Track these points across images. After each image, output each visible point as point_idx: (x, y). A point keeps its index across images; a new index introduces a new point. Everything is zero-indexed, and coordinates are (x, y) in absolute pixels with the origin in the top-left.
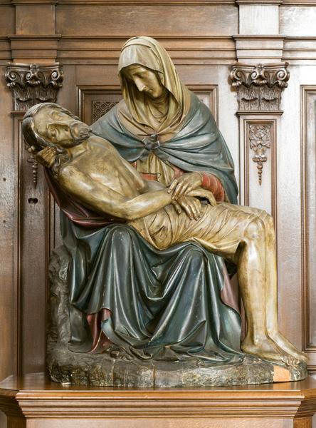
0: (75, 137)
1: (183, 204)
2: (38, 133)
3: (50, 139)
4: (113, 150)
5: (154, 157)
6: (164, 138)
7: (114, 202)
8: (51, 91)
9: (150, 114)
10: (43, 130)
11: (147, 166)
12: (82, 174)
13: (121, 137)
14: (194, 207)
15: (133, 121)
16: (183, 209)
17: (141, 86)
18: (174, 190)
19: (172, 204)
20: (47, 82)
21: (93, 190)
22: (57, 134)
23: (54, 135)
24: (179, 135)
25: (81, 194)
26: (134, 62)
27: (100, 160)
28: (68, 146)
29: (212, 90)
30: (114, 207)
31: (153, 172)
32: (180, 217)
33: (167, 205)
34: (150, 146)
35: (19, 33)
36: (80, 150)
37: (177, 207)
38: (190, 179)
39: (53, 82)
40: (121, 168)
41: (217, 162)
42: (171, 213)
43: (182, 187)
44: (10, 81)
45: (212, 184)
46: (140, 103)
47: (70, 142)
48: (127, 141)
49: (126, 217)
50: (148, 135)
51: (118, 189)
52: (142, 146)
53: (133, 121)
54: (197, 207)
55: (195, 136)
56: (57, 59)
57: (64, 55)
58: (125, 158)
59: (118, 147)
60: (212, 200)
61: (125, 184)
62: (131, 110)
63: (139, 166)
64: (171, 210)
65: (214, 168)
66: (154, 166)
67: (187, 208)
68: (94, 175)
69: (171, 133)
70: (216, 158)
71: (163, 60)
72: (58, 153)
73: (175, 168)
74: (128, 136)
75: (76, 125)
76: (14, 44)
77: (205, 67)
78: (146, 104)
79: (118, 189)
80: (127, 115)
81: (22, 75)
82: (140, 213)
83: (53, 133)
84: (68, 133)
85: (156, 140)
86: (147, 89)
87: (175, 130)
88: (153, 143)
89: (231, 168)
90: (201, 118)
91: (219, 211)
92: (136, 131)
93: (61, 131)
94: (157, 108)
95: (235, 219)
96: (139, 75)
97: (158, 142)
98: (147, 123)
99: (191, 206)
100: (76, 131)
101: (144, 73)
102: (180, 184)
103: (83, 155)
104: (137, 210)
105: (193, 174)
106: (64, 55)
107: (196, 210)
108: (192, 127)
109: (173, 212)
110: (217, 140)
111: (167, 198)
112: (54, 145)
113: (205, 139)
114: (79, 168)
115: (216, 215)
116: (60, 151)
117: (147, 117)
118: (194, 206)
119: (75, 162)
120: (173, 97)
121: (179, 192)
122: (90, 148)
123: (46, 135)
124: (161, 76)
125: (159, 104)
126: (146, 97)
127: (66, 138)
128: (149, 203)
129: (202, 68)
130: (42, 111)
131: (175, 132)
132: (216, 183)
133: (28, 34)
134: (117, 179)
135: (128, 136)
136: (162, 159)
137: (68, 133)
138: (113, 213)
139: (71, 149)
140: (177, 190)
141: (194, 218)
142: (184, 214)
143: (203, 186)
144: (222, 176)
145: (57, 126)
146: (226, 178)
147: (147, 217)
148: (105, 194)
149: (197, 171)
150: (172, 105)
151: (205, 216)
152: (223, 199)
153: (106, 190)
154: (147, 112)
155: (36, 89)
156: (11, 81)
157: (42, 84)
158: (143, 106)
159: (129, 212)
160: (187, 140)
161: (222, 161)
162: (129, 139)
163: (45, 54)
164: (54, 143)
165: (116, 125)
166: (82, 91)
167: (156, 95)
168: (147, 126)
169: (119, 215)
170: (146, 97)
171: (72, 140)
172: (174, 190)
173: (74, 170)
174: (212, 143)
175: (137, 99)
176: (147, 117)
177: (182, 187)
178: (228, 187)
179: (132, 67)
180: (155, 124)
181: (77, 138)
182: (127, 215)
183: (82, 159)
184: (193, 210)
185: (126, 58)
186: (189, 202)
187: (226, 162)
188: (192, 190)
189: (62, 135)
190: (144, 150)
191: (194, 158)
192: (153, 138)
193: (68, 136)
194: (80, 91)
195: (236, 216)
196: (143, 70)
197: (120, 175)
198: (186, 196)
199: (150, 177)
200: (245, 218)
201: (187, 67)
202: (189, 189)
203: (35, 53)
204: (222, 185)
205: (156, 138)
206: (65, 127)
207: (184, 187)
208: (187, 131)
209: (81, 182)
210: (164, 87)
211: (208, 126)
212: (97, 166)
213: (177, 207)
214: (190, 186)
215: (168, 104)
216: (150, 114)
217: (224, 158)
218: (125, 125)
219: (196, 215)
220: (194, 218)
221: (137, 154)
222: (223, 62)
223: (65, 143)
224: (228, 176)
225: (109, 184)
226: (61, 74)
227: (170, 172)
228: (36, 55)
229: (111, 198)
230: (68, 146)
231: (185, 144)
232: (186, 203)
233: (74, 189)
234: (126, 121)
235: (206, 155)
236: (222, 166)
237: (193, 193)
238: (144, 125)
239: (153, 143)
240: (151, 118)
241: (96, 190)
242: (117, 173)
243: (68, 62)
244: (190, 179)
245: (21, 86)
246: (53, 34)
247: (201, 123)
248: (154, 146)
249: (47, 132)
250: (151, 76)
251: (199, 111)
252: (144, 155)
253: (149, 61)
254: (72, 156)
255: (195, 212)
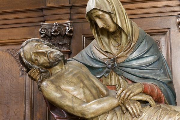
0: (51, 60)
1: (127, 106)
2: (26, 59)
3: (34, 63)
4: (85, 70)
5: (114, 73)
6: (120, 60)
7: (75, 105)
8: (66, 39)
9: (111, 44)
10: (29, 57)
11: (109, 80)
12: (54, 86)
13: (93, 61)
14: (134, 108)
15: (100, 50)
16: (127, 109)
17: (100, 24)
18: (120, 95)
19: (119, 106)
20: (64, 33)
21: (61, 97)
22: (39, 59)
23: (37, 60)
24: (131, 57)
25: (53, 100)
26: (94, 8)
27: (71, 75)
28: (48, 67)
29: (167, 32)
30: (75, 109)
31: (113, 84)
32: (126, 116)
33: (117, 107)
34: (110, 66)
35: (49, 5)
36: (58, 69)
37: (123, 108)
38: (133, 87)
39: (67, 33)
40: (86, 82)
41: (159, 75)
42: (119, 113)
43: (126, 94)
44: (42, 34)
45: (152, 91)
46: (105, 37)
47: (48, 65)
48: (96, 64)
49: (84, 116)
50: (109, 59)
51: (81, 96)
52: (105, 66)
53: (100, 50)
54: (137, 108)
55: (142, 58)
56: (70, 19)
57: (75, 16)
58: (95, 75)
59: (91, 68)
60: (152, 102)
61: (88, 92)
62: (98, 42)
63: (104, 80)
64: (119, 111)
65: (155, 79)
66: (114, 79)
67: (129, 109)
68: (63, 87)
69: (124, 56)
70: (158, 72)
71: (114, 5)
72: (41, 72)
73: (128, 81)
74: (96, 60)
75: (52, 52)
76: (45, 12)
77: (162, 18)
78: (109, 38)
79: (81, 96)
80: (97, 46)
81: (50, 30)
82: (94, 113)
83: (36, 58)
84: (46, 58)
85: (114, 62)
86: (105, 26)
87: (127, 54)
88: (112, 64)
89: (169, 80)
90: (146, 45)
91: (154, 111)
92: (102, 57)
93: (41, 57)
94: (115, 40)
95: (167, 116)
96: (98, 17)
97: (116, 62)
98: (108, 50)
99: (133, 107)
100: (52, 56)
101: (101, 15)
102: (125, 91)
103: (59, 73)
104: (92, 111)
105: (136, 84)
106: (75, 16)
107: (136, 110)
108: (140, 51)
109: (120, 112)
110: (158, 60)
111: (115, 102)
112: (37, 67)
113: (150, 59)
114: (52, 82)
115: (152, 114)
116: (43, 71)
117: (109, 47)
118: (135, 107)
119: (52, 78)
120: (124, 31)
121: (124, 96)
122: (66, 68)
123: (31, 60)
124: (113, 15)
125: (116, 37)
126: (104, 32)
127: (45, 62)
128: (100, 106)
129: (159, 18)
130: (29, 44)
131: (127, 55)
132: (156, 90)
133: (53, 5)
134: (81, 90)
135: (97, 60)
136: (118, 75)
137: (46, 58)
138: (75, 114)
139: (51, 70)
140: (122, 96)
141: (135, 116)
142: (128, 113)
143: (144, 92)
144: (162, 85)
145: (38, 53)
146: (165, 87)
147: (101, 116)
148: (69, 99)
149: (140, 82)
150: (124, 36)
151: (144, 114)
152: (164, 102)
153: (70, 97)
154: (109, 43)
155: (58, 37)
156: (42, 34)
157: (60, 34)
158: (106, 39)
159: (86, 113)
160: (136, 61)
161: (162, 75)
162: (98, 62)
163: (63, 16)
164: (38, 65)
165: (89, 52)
166: (86, 37)
167: (111, 30)
168: (109, 52)
169: (80, 115)
170: (104, 32)
171: (50, 63)
172: (120, 95)
173: (49, 84)
174: (154, 62)
175: (103, 35)
176: (109, 47)
177: (126, 94)
178: (167, 93)
179: (93, 11)
180: (114, 51)
181: (53, 61)
182: (84, 115)
183: (57, 76)
184: (134, 110)
185: (89, 6)
186: (131, 105)
187: (166, 75)
188: (134, 96)
189: (42, 60)
190: (107, 69)
191: (142, 73)
192: (112, 60)
193: (46, 60)
194: (85, 38)
195: (167, 114)
196: (101, 13)
197: (85, 86)
198: (130, 100)
199: (112, 88)
200: (175, 115)
201: (150, 19)
202: (132, 95)
203: (58, 17)
204: (161, 91)
205: (114, 60)
206: (44, 54)
207: (128, 94)
208: (135, 55)
209: (53, 92)
210: (116, 24)
211: (151, 50)
212: (67, 80)
213: (123, 108)
214: (135, 91)
215: (121, 37)
216: (111, 44)
217: (164, 73)
218: (95, 53)
219: (136, 114)
220: (135, 116)
221: (102, 72)
222: (173, 14)
223: (45, 65)
224: (167, 85)
225: (75, 93)
226: (71, 28)
227: (125, 84)
228: (57, 18)
229: (73, 102)
230: (48, 67)
231: (135, 63)
232: (129, 105)
233: (48, 97)
234: (97, 50)
235: (151, 71)
236: (162, 78)
237: (135, 97)
238: (107, 52)
239: (112, 64)
240: (112, 47)
241: (63, 97)
242: (82, 85)
243: (77, 21)
244: (133, 87)
245: (49, 37)
246: (67, 4)
247: (146, 48)
248: (113, 66)
249: (31, 58)
250: (107, 16)
251: (144, 41)
252: (107, 72)
253: (104, 6)
254: (52, 74)
255: (135, 112)
